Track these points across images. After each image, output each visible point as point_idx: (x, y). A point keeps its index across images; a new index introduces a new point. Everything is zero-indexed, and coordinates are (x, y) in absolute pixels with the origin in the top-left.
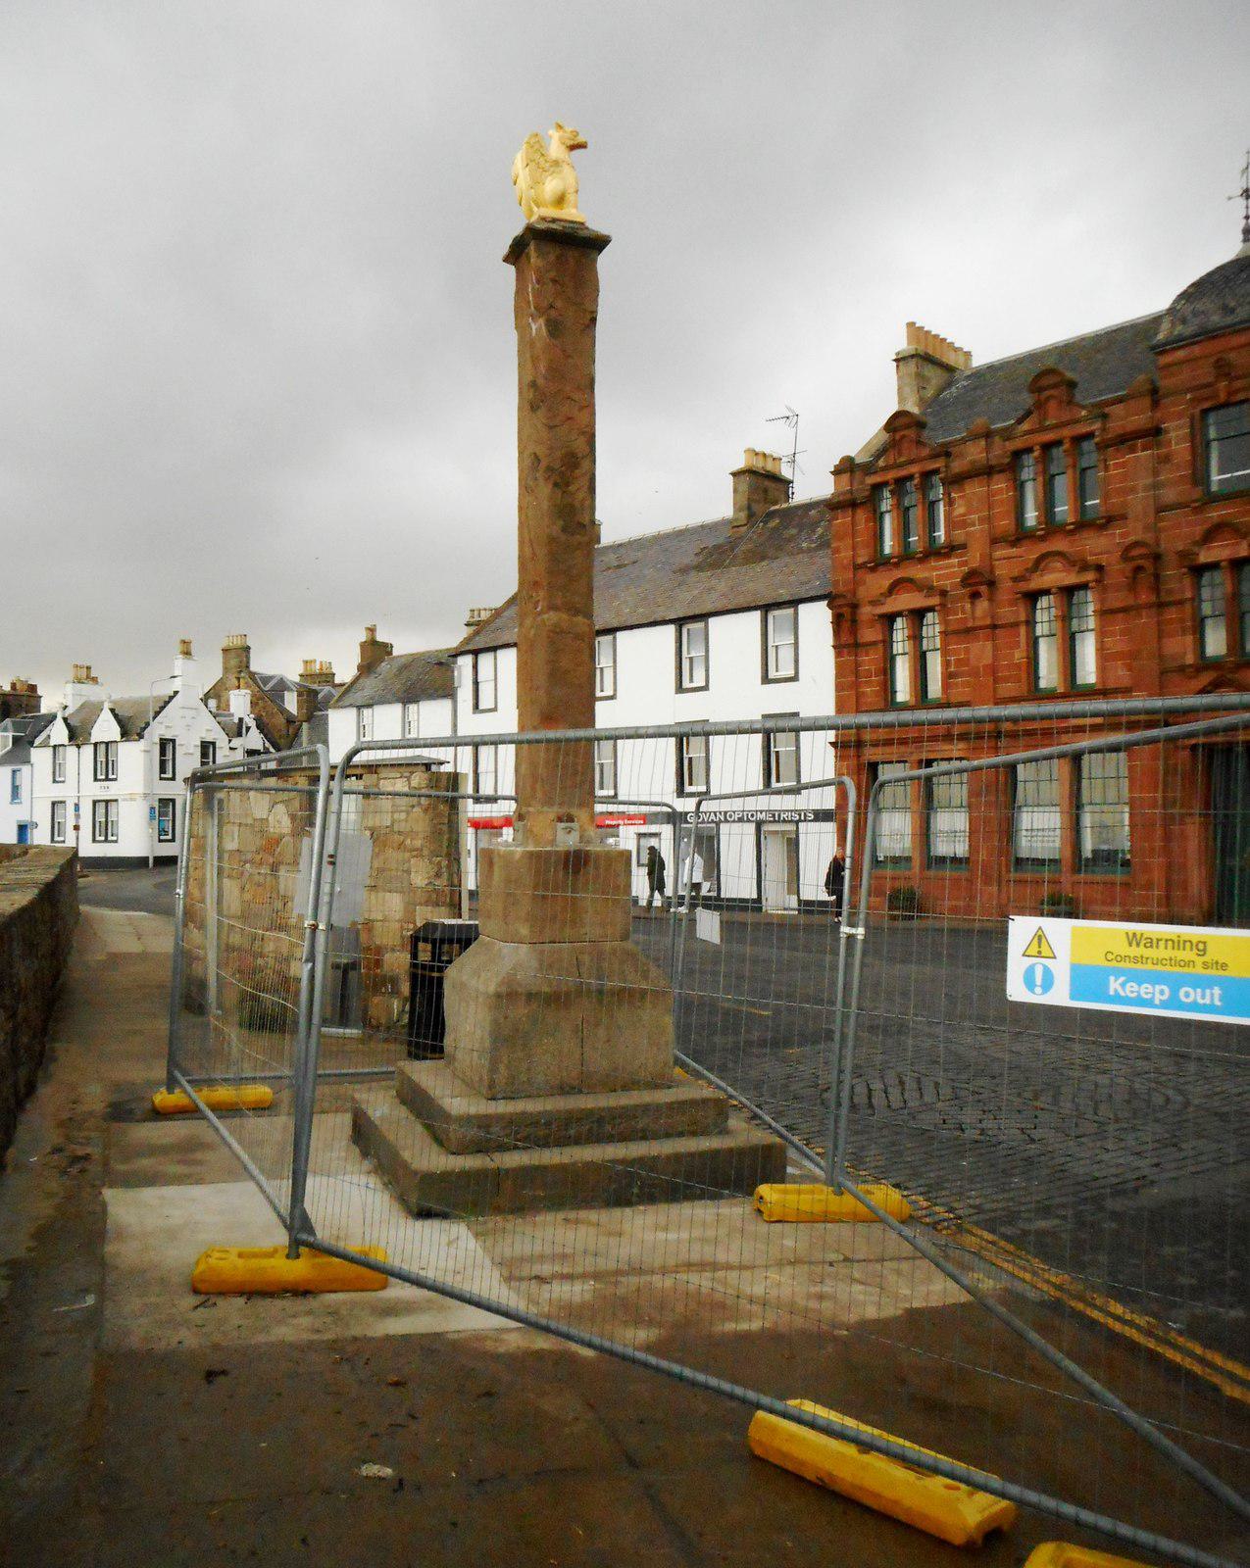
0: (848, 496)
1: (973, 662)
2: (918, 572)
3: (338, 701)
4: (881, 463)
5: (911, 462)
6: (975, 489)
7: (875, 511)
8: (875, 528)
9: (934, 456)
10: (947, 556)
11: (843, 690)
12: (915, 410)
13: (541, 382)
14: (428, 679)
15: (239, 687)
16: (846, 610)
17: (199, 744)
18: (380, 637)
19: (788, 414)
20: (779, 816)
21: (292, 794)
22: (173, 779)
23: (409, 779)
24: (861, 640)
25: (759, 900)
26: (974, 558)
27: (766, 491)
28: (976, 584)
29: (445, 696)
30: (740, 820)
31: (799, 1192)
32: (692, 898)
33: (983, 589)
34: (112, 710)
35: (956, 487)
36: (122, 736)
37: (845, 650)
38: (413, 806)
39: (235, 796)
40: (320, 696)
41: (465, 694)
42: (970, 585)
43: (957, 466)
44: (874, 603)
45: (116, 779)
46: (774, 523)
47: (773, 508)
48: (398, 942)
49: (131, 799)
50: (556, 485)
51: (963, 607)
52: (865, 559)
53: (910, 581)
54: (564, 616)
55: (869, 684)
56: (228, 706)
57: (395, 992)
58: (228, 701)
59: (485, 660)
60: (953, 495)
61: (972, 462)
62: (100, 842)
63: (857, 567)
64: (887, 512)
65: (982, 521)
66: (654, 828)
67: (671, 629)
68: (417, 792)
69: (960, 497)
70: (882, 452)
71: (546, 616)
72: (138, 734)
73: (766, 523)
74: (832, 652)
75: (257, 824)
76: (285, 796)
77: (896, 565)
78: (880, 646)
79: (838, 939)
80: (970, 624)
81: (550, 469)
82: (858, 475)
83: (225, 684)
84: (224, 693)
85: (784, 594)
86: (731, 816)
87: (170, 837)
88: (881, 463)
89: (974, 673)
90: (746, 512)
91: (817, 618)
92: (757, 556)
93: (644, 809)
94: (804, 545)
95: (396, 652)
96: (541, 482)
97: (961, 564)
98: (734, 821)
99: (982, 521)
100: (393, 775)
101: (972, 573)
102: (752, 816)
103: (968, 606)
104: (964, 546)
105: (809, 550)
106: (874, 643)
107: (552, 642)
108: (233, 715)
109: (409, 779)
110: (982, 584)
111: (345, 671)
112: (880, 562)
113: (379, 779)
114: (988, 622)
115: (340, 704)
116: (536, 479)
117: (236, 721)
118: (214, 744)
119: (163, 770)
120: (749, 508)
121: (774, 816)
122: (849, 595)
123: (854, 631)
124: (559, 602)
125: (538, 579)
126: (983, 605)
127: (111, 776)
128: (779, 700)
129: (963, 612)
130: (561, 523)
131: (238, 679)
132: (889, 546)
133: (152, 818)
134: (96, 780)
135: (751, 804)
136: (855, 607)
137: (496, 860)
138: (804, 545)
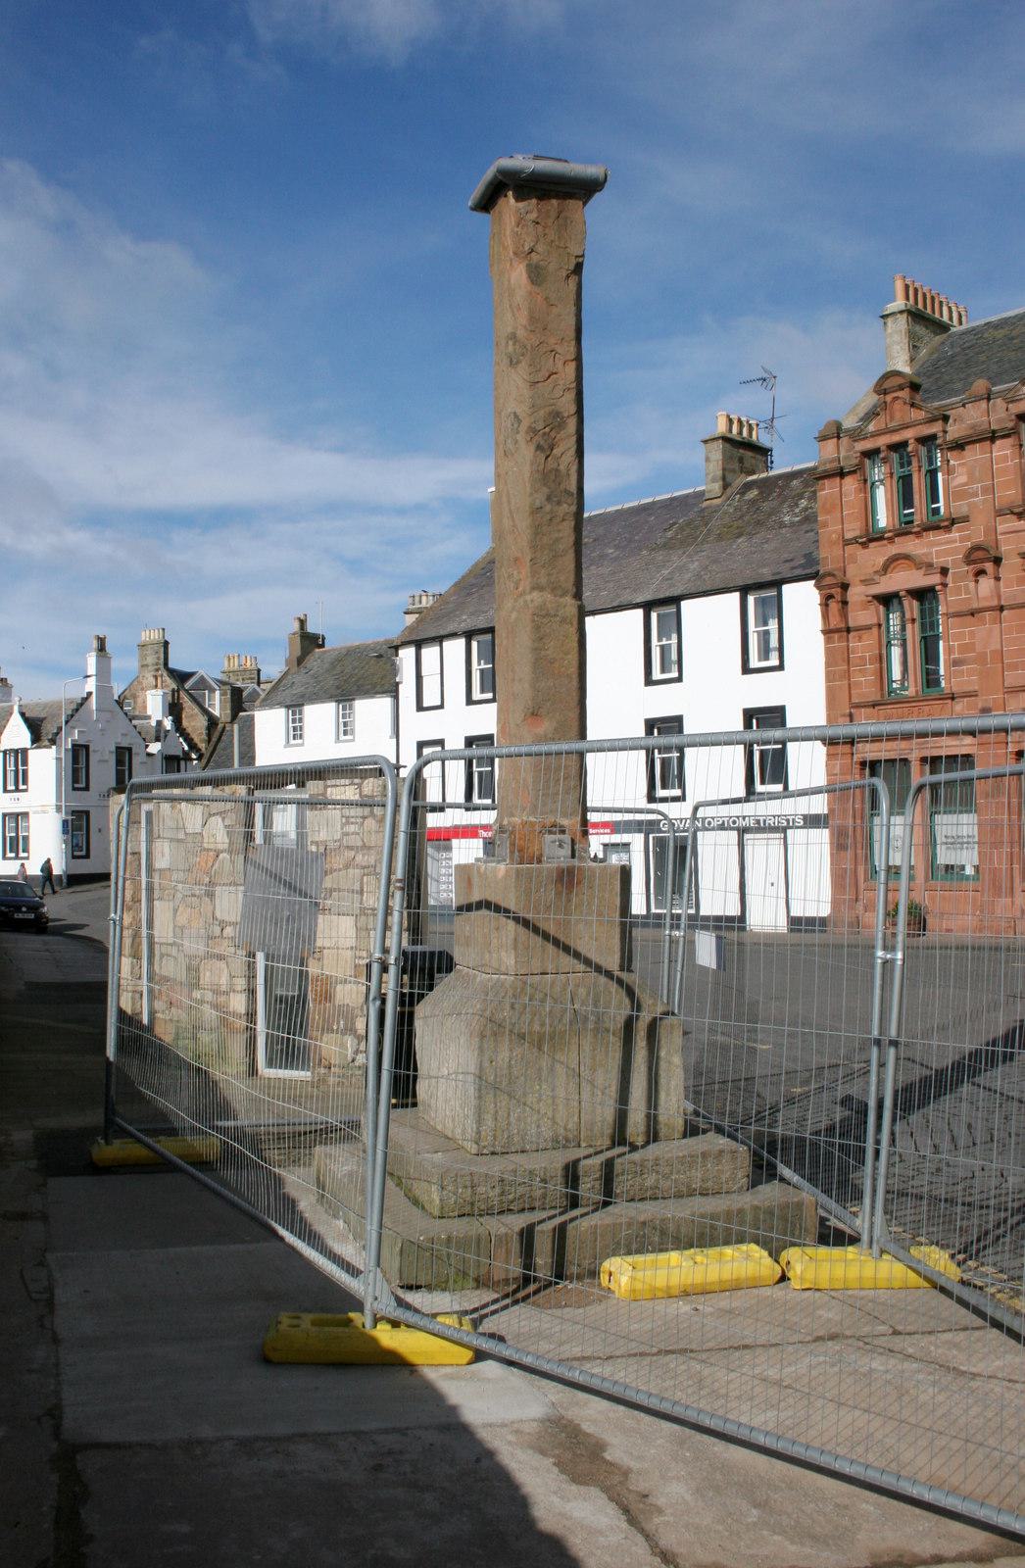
0: (836, 464)
1: (979, 648)
2: (910, 546)
3: (264, 700)
4: (871, 428)
5: (906, 427)
6: (975, 454)
7: (865, 481)
8: (866, 498)
9: (932, 420)
10: (948, 529)
11: (834, 680)
12: (907, 370)
13: (521, 333)
14: (365, 674)
15: (156, 686)
16: (837, 591)
17: (113, 749)
18: (311, 629)
19: (765, 375)
20: (765, 821)
21: (229, 805)
22: (87, 788)
23: (360, 786)
24: (851, 624)
25: (742, 918)
26: (976, 533)
27: (741, 460)
28: (983, 561)
29: (384, 692)
30: (722, 827)
31: (176, 1141)
32: (691, 917)
33: (989, 566)
34: (23, 715)
35: (955, 453)
36: (33, 742)
37: (836, 636)
38: (364, 818)
39: (165, 806)
40: (245, 694)
41: (407, 690)
42: (974, 562)
43: (954, 431)
44: (866, 582)
45: (26, 790)
46: (753, 493)
47: (750, 478)
48: (350, 971)
49: (44, 812)
50: (539, 447)
51: (966, 586)
52: (857, 533)
53: (907, 557)
54: (548, 596)
55: (863, 672)
56: (145, 708)
57: (350, 1030)
58: (144, 702)
59: (430, 653)
60: (952, 462)
61: (973, 427)
62: (10, 859)
63: (847, 543)
64: (881, 481)
65: (985, 491)
66: (625, 838)
67: (591, 622)
68: (370, 801)
69: (959, 465)
70: (872, 414)
71: (528, 598)
72: (49, 740)
73: (743, 494)
74: (821, 638)
75: (190, 839)
76: (221, 806)
77: (891, 540)
78: (875, 630)
79: (873, 966)
80: (975, 605)
81: (533, 431)
82: (845, 441)
83: (140, 683)
84: (140, 693)
85: (766, 574)
86: (709, 823)
87: (84, 853)
88: (871, 428)
89: (981, 659)
90: (721, 483)
91: (802, 601)
92: (736, 531)
93: (618, 817)
94: (787, 518)
95: (328, 646)
96: (522, 444)
97: (962, 539)
98: (713, 829)
99: (985, 491)
100: (343, 781)
101: (976, 548)
102: (734, 822)
103: (972, 585)
104: (965, 519)
105: (792, 524)
106: (868, 628)
107: (537, 628)
108: (149, 717)
109: (360, 786)
110: (988, 560)
111: (273, 668)
112: (872, 537)
113: (326, 787)
114: (995, 603)
115: (269, 702)
116: (516, 442)
117: (154, 724)
118: (130, 750)
119: (75, 780)
120: (724, 478)
121: (788, 821)
122: (839, 574)
123: (844, 615)
124: (543, 581)
125: (520, 555)
126: (986, 584)
127: (22, 787)
128: (763, 692)
129: (967, 592)
130: (545, 490)
131: (156, 677)
132: (883, 520)
133: (26, 839)
134: (5, 790)
135: (735, 810)
136: (845, 587)
137: (476, 880)
138: (787, 518)
